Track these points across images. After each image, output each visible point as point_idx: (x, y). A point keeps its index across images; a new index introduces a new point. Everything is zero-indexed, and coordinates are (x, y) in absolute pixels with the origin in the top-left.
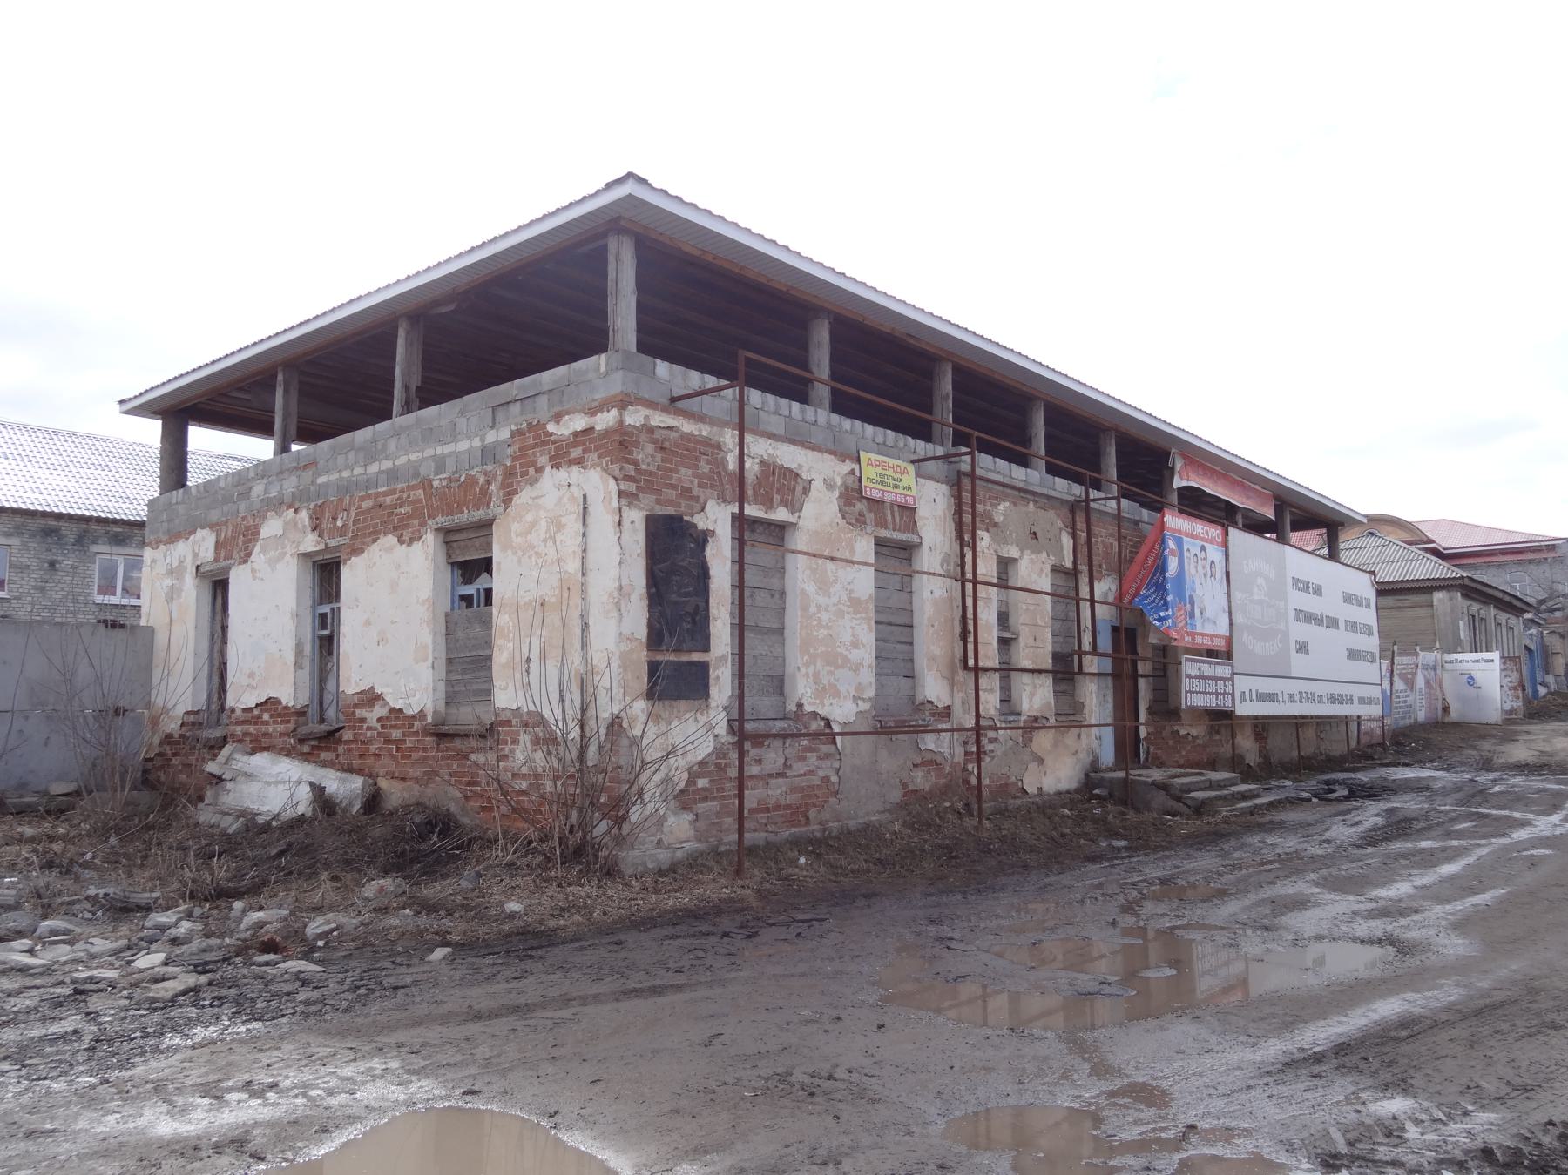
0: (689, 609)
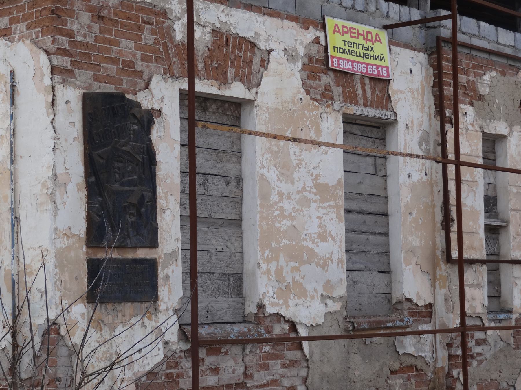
0: (134, 199)
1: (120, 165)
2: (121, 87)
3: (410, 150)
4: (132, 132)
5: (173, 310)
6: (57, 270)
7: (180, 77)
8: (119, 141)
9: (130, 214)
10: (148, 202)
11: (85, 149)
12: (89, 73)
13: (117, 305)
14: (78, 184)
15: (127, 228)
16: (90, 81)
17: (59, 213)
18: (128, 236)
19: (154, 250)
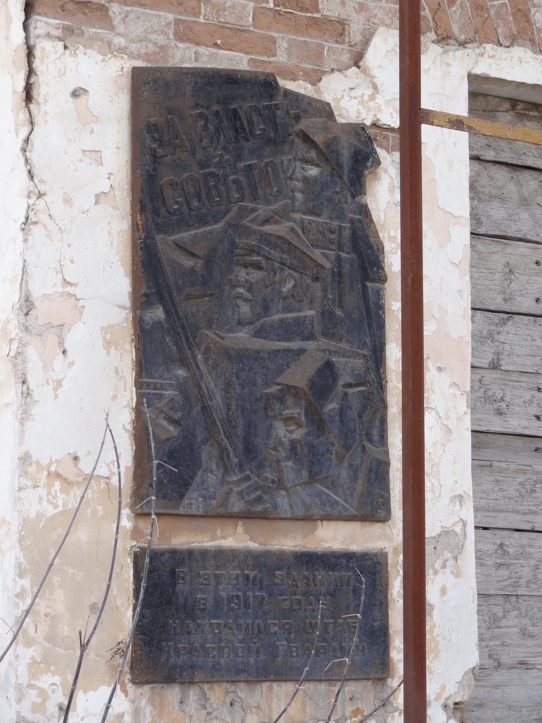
0: (299, 375)
1: (256, 275)
2: (272, 59)
3: (427, 68)
4: (299, 185)
5: (445, 706)
6: (26, 582)
7: (472, 42)
8: (253, 210)
9: (287, 420)
10: (350, 385)
11: (135, 227)
12: (160, 17)
13: (242, 691)
14: (106, 330)
15: (278, 461)
16: (161, 39)
17: (35, 411)
18: (280, 484)
19: (377, 528)
